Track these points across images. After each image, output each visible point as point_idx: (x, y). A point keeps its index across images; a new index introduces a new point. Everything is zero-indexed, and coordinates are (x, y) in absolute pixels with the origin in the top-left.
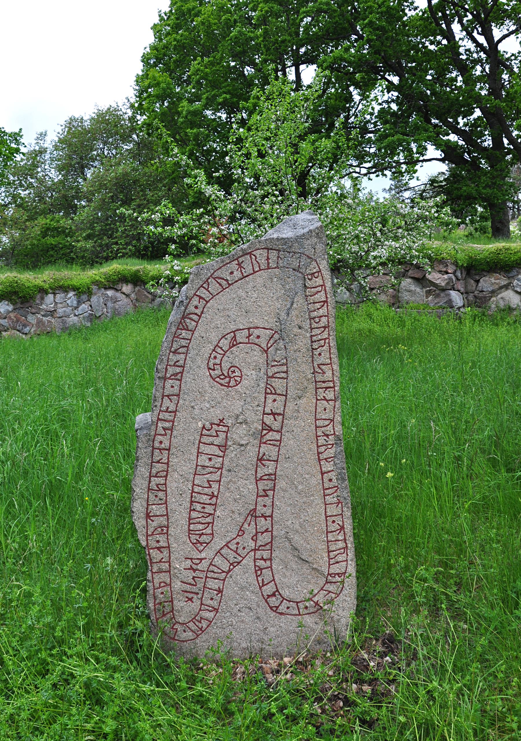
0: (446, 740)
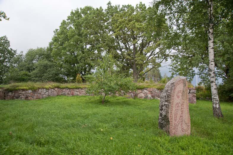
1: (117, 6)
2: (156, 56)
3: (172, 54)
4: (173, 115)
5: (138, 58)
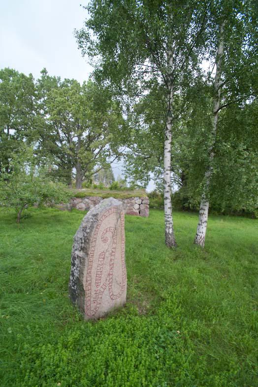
0: (251, 249)
1: (57, 78)
2: (106, 153)
3: (125, 153)
4: (94, 281)
5: (82, 154)
